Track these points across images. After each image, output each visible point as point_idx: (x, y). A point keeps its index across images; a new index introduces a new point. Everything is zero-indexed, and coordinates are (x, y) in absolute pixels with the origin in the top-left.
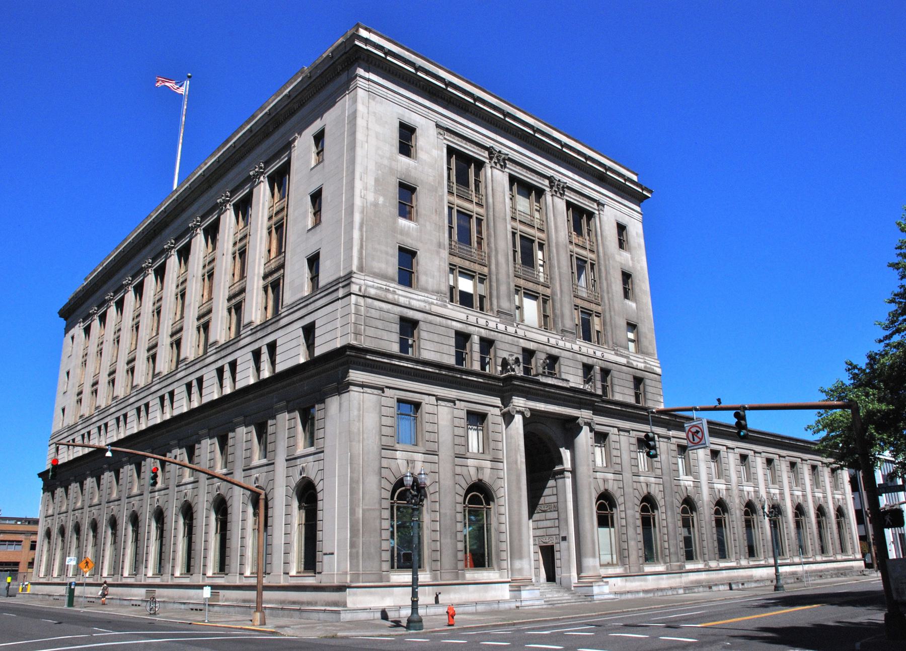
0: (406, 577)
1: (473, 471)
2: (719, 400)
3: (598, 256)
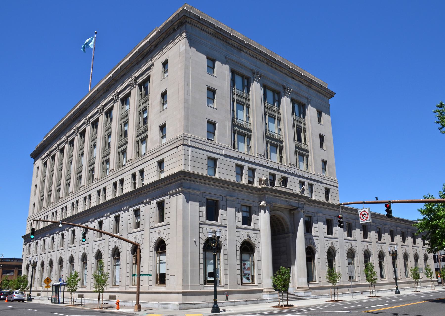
0: (211, 288)
2: (377, 198)
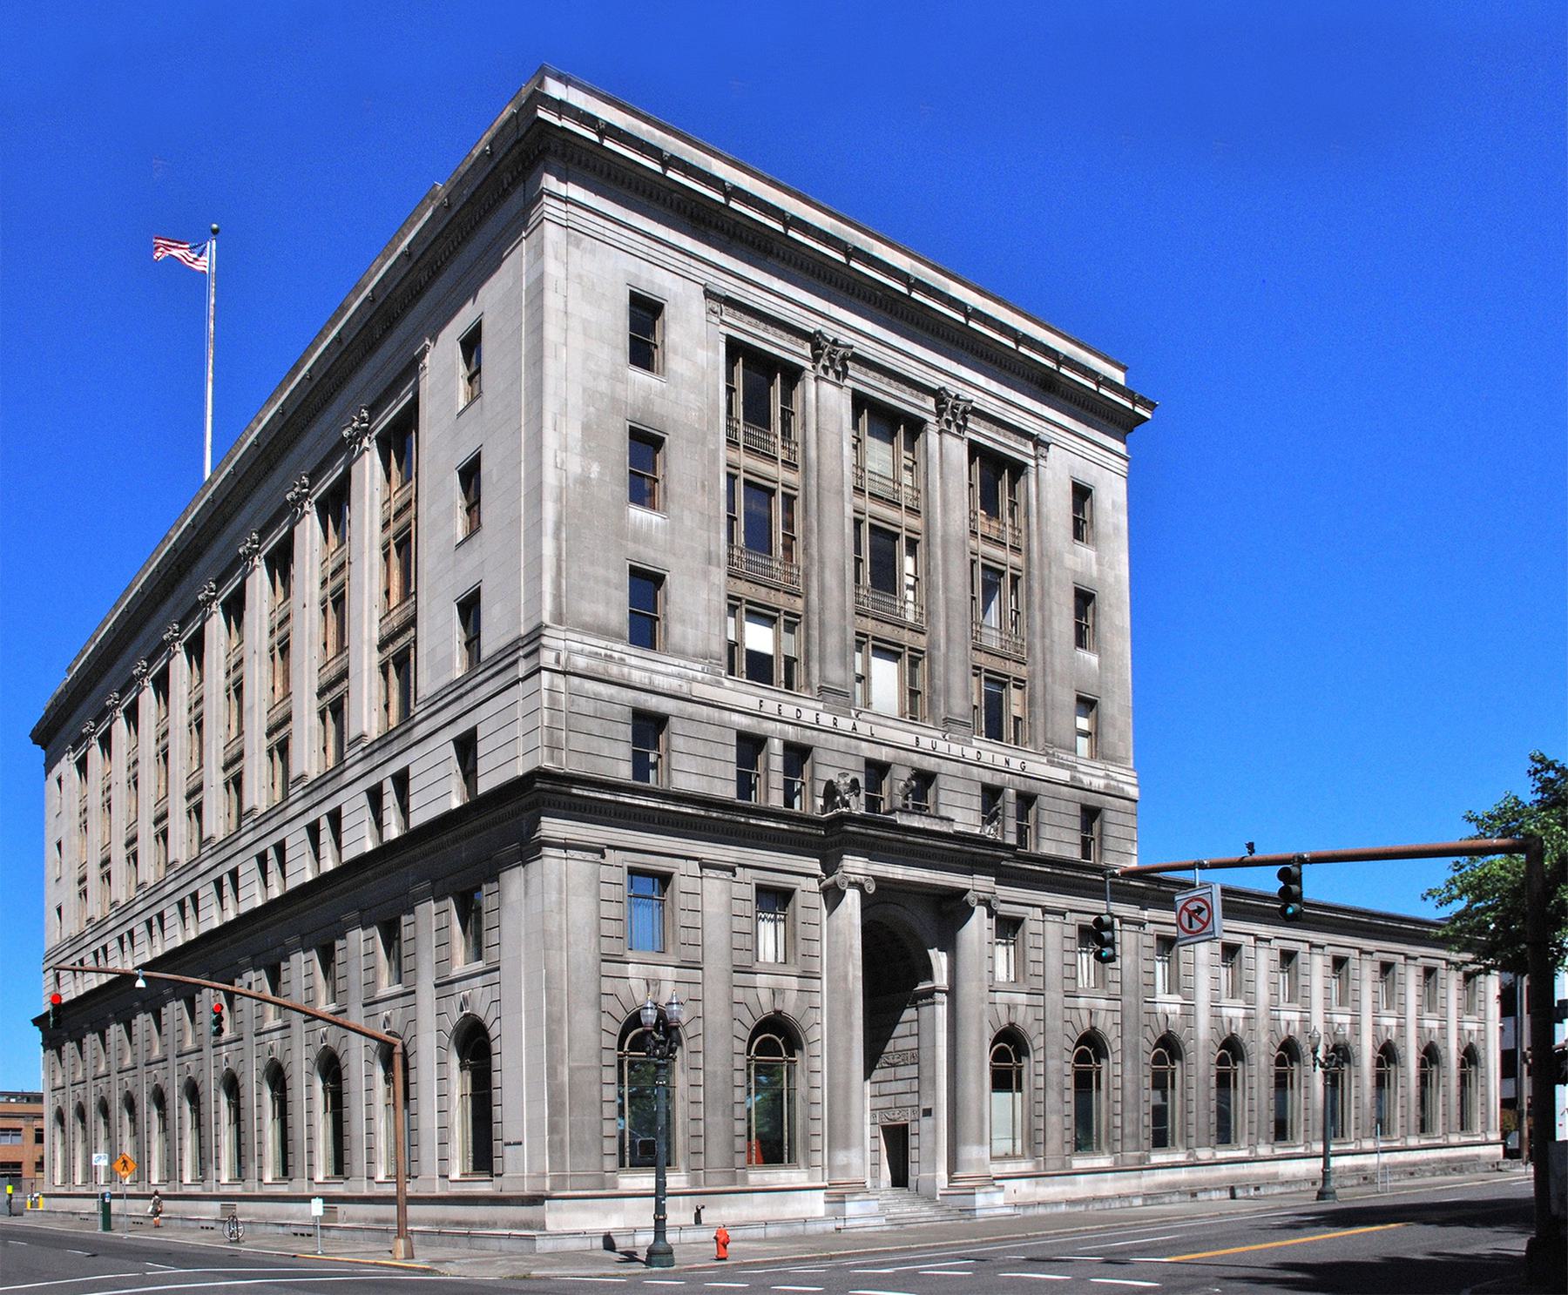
1: (765, 996)
2: (1251, 846)
3: (1028, 560)
